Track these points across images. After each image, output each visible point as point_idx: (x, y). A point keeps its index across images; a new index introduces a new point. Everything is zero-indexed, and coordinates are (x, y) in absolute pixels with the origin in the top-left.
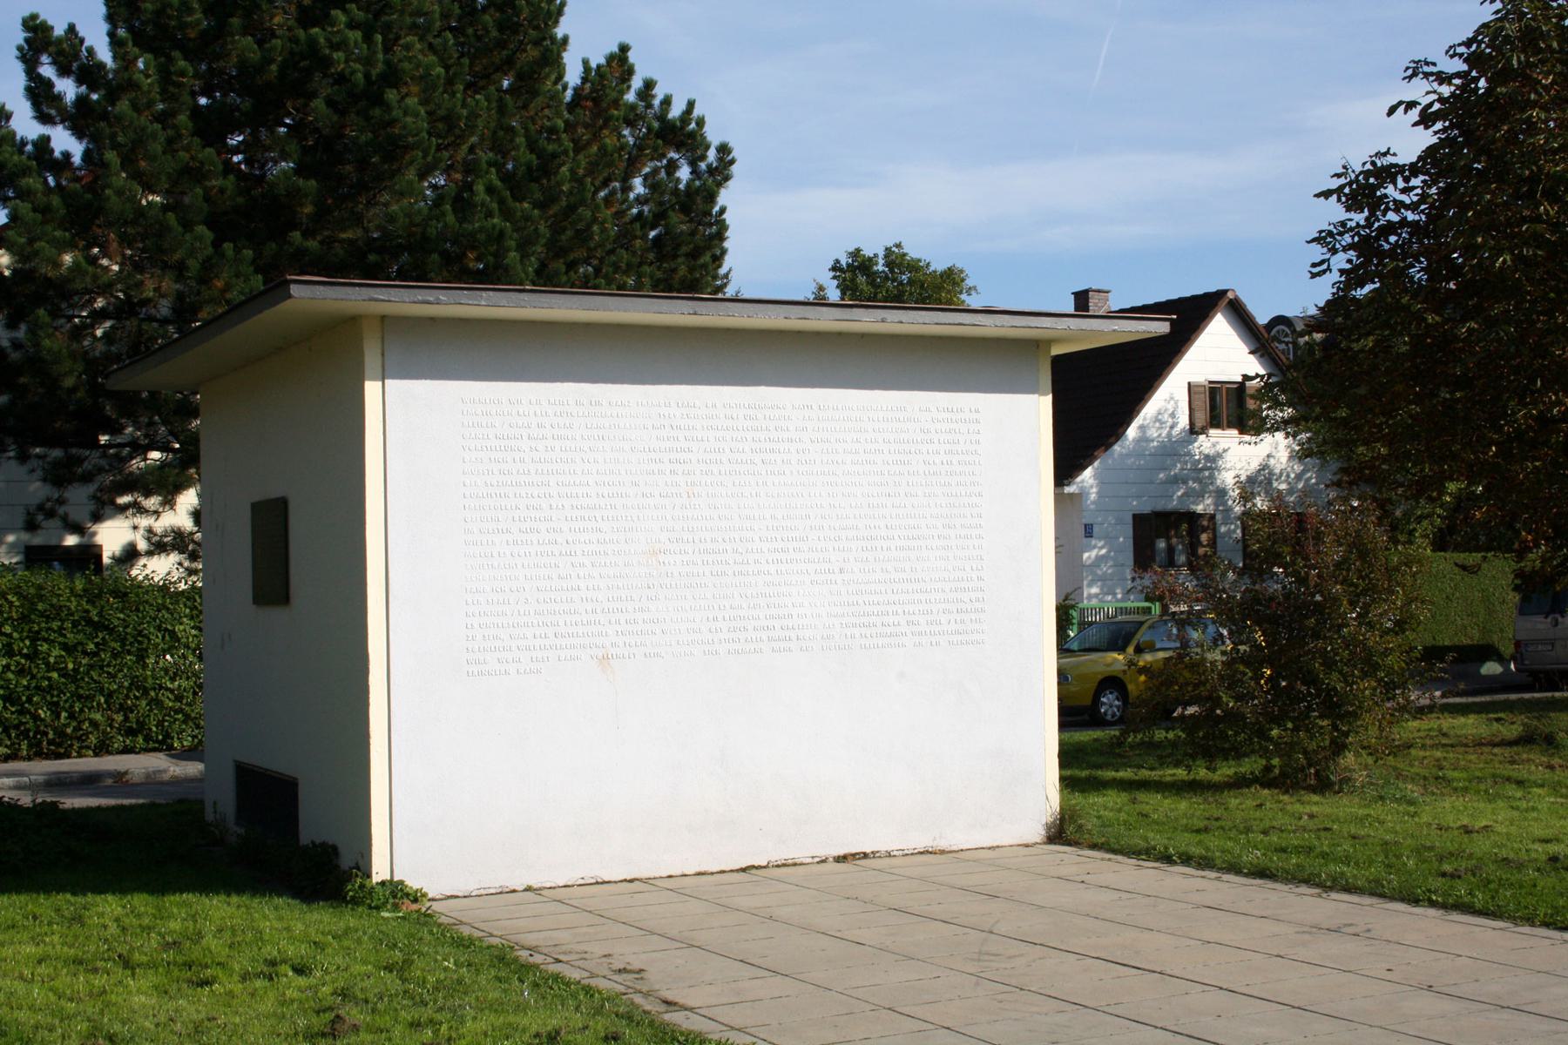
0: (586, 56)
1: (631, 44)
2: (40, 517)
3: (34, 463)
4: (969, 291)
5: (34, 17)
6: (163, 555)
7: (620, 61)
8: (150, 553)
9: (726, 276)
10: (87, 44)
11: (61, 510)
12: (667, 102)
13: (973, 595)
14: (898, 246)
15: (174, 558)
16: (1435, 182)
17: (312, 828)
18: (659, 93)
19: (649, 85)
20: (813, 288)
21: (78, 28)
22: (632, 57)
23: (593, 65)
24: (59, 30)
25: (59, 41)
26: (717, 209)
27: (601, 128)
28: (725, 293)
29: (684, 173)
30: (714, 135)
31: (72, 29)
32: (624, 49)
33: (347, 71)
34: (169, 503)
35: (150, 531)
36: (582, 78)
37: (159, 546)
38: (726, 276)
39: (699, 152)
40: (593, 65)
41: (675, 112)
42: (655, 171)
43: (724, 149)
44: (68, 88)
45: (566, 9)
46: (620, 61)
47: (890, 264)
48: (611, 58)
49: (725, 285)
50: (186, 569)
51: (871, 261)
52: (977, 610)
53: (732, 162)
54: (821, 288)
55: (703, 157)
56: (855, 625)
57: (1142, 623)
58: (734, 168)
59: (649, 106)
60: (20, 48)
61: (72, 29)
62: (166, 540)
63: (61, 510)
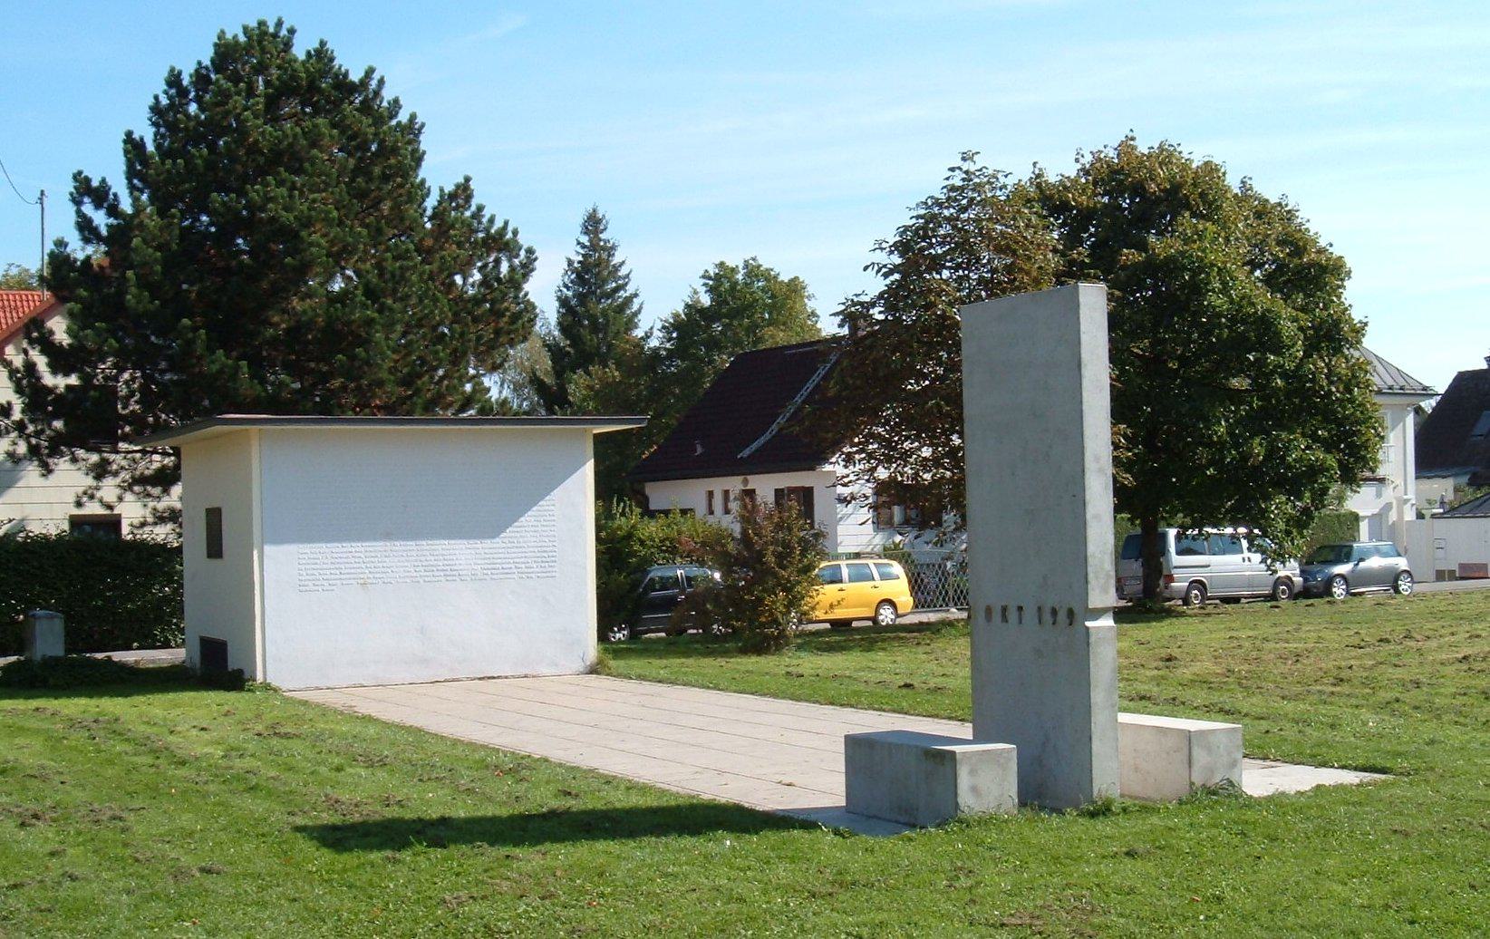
0: (441, 185)
1: (471, 176)
2: (85, 499)
3: (81, 464)
4: (809, 297)
5: (80, 173)
6: (163, 524)
7: (463, 192)
8: (155, 524)
9: (627, 276)
10: (112, 191)
11: (98, 494)
12: (492, 220)
13: (550, 554)
14: (754, 259)
15: (170, 526)
16: (1064, 266)
17: (233, 664)
18: (487, 214)
19: (480, 208)
20: (689, 291)
21: (107, 180)
22: (472, 185)
23: (446, 191)
24: (95, 183)
25: (97, 189)
26: (523, 293)
27: (444, 243)
28: (626, 291)
29: (504, 268)
30: (524, 240)
31: (104, 180)
32: (467, 179)
33: (277, 216)
34: (166, 491)
35: (155, 509)
36: (439, 201)
37: (160, 519)
38: (627, 276)
39: (514, 253)
40: (446, 191)
41: (498, 224)
42: (485, 266)
43: (530, 251)
44: (100, 219)
45: (425, 157)
46: (463, 192)
47: (748, 275)
48: (458, 186)
49: (626, 284)
50: (178, 534)
51: (734, 270)
52: (553, 562)
53: (536, 259)
54: (696, 292)
55: (517, 256)
56: (488, 569)
57: (873, 579)
58: (536, 263)
59: (480, 223)
60: (71, 194)
61: (104, 180)
62: (165, 515)
63: (98, 494)
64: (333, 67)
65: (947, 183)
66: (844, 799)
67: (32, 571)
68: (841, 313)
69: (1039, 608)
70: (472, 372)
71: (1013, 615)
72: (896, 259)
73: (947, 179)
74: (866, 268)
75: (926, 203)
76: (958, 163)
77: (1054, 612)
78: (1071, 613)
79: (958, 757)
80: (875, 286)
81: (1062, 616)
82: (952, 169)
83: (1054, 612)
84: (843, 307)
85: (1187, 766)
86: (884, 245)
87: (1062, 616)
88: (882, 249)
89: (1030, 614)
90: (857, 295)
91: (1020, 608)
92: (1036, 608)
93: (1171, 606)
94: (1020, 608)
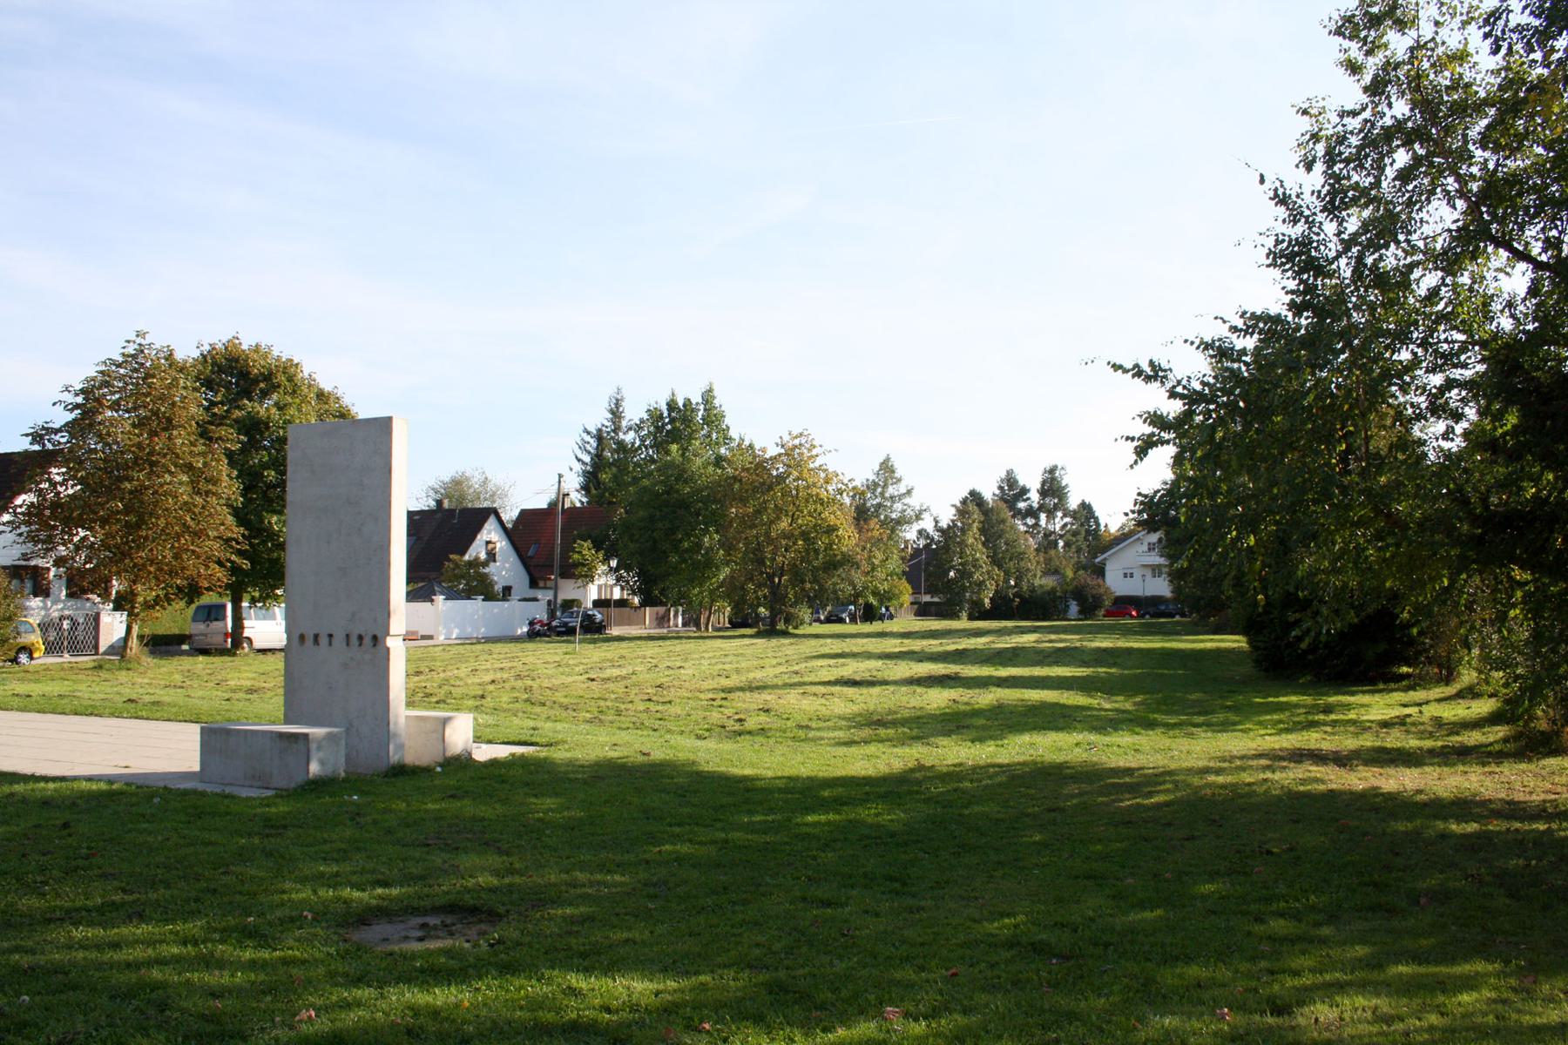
64: (1260, 340)
65: (123, 351)
66: (199, 764)
67: (1282, 904)
68: (31, 434)
69: (347, 636)
70: (1017, 600)
71: (324, 640)
72: (80, 400)
73: (124, 348)
74: (54, 404)
75: (105, 362)
76: (133, 337)
77: (360, 638)
78: (375, 638)
79: (311, 737)
80: (62, 417)
81: (367, 641)
82: (128, 342)
83: (360, 638)
84: (33, 430)
85: (517, 739)
86: (70, 389)
87: (367, 641)
88: (69, 391)
89: (339, 641)
90: (46, 423)
91: (330, 636)
92: (344, 635)
93: (117, 592)
94: (330, 636)
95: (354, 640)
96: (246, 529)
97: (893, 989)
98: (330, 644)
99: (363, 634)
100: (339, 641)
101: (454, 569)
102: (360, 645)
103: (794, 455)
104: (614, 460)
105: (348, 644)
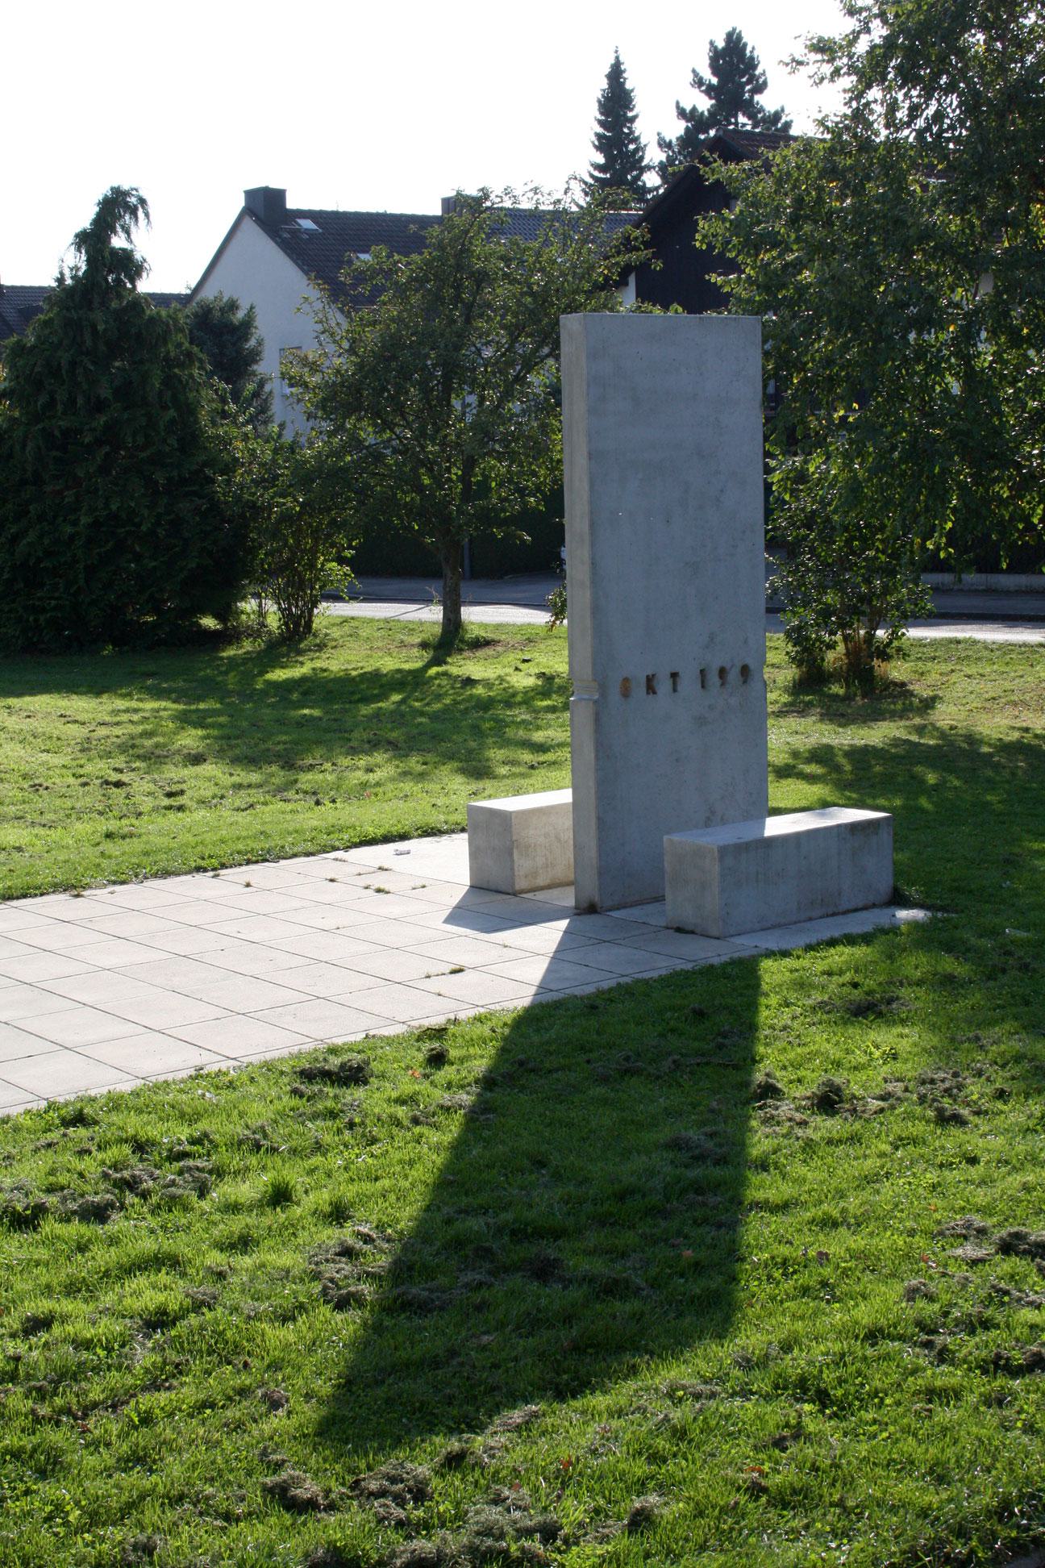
69: (702, 671)
71: (664, 686)
77: (722, 672)
78: (745, 671)
81: (734, 675)
83: (722, 672)
87: (734, 675)
89: (688, 682)
91: (674, 675)
94: (674, 675)
95: (714, 679)
96: (711, 184)
97: (816, 1373)
98: (675, 690)
99: (728, 667)
100: (688, 682)
101: (320, 1444)
102: (723, 684)
103: (459, 194)
104: (302, 505)
105: (703, 687)
